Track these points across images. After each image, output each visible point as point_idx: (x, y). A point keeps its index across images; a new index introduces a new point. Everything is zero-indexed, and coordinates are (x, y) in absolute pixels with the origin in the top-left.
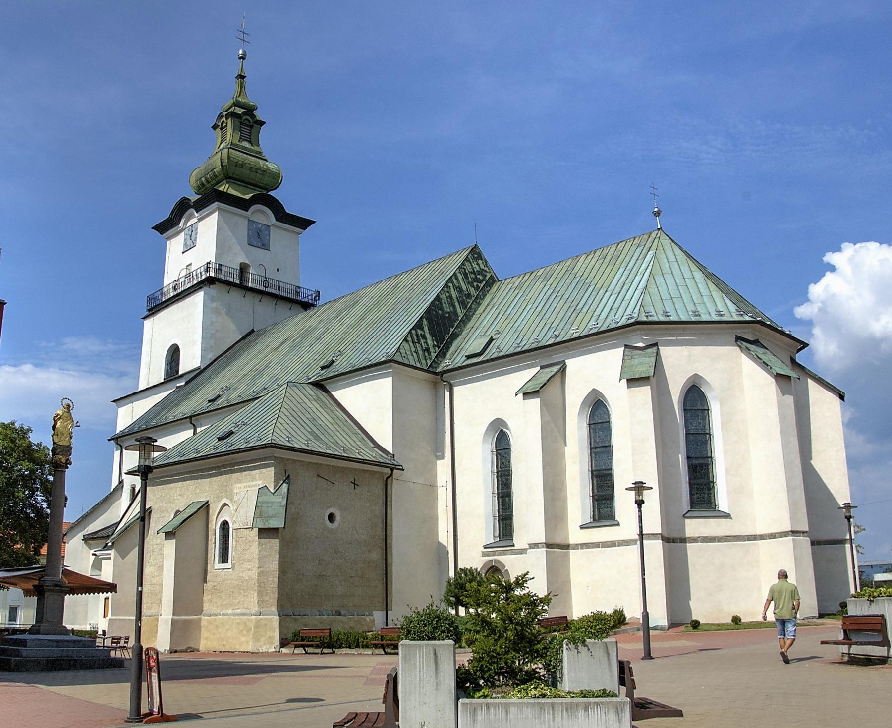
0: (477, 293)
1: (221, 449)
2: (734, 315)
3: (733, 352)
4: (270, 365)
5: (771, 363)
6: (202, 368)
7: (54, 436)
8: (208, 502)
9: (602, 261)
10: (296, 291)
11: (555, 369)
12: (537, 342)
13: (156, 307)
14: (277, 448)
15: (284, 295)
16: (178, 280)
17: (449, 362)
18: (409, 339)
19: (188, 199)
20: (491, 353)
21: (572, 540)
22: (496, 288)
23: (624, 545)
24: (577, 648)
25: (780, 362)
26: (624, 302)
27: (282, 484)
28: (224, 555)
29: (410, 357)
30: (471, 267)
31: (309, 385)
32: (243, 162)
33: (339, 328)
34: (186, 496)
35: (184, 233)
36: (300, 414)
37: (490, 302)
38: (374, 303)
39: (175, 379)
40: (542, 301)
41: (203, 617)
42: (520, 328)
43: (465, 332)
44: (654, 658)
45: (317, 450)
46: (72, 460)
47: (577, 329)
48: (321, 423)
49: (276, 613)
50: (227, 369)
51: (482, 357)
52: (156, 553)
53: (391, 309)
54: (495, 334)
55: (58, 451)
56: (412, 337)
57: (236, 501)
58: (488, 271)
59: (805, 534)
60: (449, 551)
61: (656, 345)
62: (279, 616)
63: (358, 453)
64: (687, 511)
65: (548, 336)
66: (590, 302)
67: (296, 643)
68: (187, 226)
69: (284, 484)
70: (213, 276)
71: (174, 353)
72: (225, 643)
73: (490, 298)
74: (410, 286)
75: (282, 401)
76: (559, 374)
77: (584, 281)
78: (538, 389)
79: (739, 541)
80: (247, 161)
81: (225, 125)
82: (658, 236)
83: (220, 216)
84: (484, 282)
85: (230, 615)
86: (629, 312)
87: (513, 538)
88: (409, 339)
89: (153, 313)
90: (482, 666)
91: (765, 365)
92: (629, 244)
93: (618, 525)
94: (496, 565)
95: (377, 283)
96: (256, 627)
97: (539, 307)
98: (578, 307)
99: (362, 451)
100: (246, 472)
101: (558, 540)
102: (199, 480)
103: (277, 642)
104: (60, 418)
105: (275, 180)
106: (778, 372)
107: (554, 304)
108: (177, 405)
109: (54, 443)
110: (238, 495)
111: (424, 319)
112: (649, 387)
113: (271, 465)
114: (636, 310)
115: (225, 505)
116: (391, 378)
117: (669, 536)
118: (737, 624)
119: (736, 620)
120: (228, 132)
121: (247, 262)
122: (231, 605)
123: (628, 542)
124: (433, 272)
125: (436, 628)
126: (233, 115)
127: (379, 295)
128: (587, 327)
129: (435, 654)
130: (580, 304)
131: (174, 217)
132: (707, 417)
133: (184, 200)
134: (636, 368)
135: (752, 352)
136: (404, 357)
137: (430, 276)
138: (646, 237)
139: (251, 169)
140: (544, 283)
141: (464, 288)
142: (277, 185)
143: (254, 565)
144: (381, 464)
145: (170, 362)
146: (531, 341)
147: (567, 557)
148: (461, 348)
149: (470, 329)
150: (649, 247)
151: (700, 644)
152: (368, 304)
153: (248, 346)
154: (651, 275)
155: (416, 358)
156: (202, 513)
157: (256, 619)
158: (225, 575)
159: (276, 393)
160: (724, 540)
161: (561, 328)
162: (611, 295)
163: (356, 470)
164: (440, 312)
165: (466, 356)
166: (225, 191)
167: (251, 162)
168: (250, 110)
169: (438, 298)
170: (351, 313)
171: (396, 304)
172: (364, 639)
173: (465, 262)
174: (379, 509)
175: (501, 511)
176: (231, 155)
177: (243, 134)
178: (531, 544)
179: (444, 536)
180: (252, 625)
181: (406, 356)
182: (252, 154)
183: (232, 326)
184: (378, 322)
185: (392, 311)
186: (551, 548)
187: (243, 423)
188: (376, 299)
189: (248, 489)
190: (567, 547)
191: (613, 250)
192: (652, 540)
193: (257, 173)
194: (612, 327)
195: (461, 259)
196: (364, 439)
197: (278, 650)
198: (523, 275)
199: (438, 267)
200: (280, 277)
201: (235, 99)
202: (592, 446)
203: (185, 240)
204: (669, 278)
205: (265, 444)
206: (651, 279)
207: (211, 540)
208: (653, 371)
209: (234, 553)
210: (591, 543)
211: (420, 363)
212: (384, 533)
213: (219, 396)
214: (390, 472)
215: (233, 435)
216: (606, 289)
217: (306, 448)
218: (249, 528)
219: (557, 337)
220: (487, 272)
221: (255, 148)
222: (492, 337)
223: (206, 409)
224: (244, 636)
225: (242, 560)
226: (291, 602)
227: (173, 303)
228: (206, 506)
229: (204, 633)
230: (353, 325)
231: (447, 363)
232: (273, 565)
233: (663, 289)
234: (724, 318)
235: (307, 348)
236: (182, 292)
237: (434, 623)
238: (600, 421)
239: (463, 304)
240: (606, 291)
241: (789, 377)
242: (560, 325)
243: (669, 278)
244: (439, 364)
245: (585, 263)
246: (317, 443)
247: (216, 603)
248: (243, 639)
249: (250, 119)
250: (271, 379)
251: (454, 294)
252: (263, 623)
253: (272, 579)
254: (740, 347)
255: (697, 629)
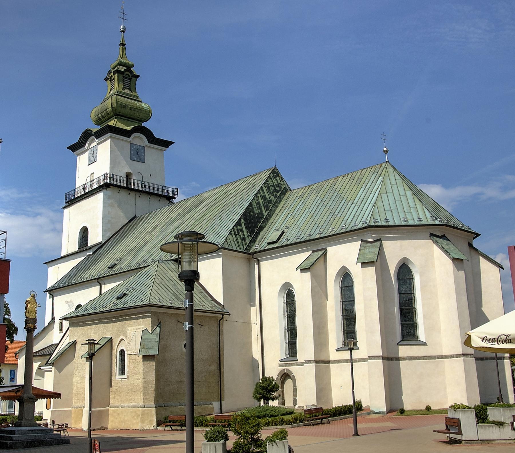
0: (276, 199)
1: (119, 306)
2: (429, 220)
3: (429, 243)
4: (147, 244)
5: (451, 251)
6: (103, 242)
7: (26, 313)
8: (111, 338)
9: (352, 181)
10: (163, 189)
11: (321, 253)
12: (310, 236)
13: (72, 201)
14: (153, 306)
15: (155, 192)
16: (85, 184)
17: (257, 247)
18: (233, 233)
19: (91, 130)
20: (283, 242)
21: (332, 358)
22: (287, 195)
23: (362, 362)
24: (272, 444)
25: (457, 249)
26: (362, 211)
27: (156, 327)
28: (122, 370)
29: (233, 245)
30: (272, 182)
31: (172, 261)
32: (126, 104)
33: (190, 221)
34: (98, 334)
35: (88, 152)
36: (166, 282)
37: (284, 205)
38: (212, 204)
39: (86, 250)
40: (315, 207)
41: (110, 408)
42: (301, 225)
43: (268, 226)
44: (359, 435)
45: (177, 306)
46: (37, 326)
47: (333, 229)
48: (179, 287)
49: (154, 406)
50: (119, 245)
51: (277, 244)
52: (80, 369)
53: (222, 210)
54: (285, 229)
55: (29, 321)
56: (234, 231)
57: (129, 338)
58: (283, 184)
59: (472, 355)
60: (260, 363)
61: (380, 240)
62: (156, 407)
63: (202, 306)
64: (400, 341)
65: (316, 232)
66: (342, 210)
67: (166, 424)
68: (90, 147)
69: (157, 327)
70: (109, 182)
71: (84, 232)
72: (123, 424)
73: (284, 203)
74: (234, 193)
75: (155, 274)
76: (323, 256)
77: (340, 194)
78: (309, 267)
79: (432, 359)
80: (128, 104)
81: (113, 78)
82: (386, 166)
83: (112, 142)
84: (280, 192)
85: (126, 407)
86: (364, 219)
87: (297, 355)
88: (233, 233)
89: (69, 205)
90: (236, 450)
91: (446, 252)
92: (369, 170)
93: (358, 349)
94: (287, 372)
95: (214, 189)
96: (142, 414)
97: (312, 211)
98: (335, 214)
99: (205, 304)
100: (135, 320)
101: (323, 358)
102: (106, 324)
103: (155, 423)
104: (30, 302)
105: (147, 115)
106: (454, 257)
107: (322, 210)
108: (88, 268)
109: (26, 317)
110: (130, 334)
111: (242, 219)
112: (374, 267)
113: (149, 316)
114: (369, 218)
115: (122, 340)
116: (221, 258)
117: (388, 357)
118: (429, 411)
119: (428, 408)
120: (115, 83)
121: (131, 171)
122: (127, 401)
123: (364, 360)
124: (249, 185)
125: (218, 435)
126: (118, 72)
127: (215, 199)
128: (339, 228)
129: (215, 447)
130: (336, 211)
131: (82, 141)
132: (412, 283)
133: (88, 130)
134: (367, 255)
135: (439, 244)
136: (230, 245)
137: (247, 187)
138: (379, 166)
139: (131, 109)
140: (316, 194)
141: (267, 196)
142: (148, 118)
143: (140, 376)
144: (216, 312)
145: (82, 237)
146: (306, 235)
147: (329, 368)
148: (265, 236)
149: (270, 224)
150: (380, 174)
151: (395, 425)
152: (208, 204)
153: (133, 228)
154: (380, 194)
155: (237, 245)
156: (108, 345)
157: (142, 410)
158: (123, 382)
159: (152, 268)
160: (422, 359)
161: (325, 227)
162: (355, 206)
163: (200, 316)
164: (252, 214)
165: (268, 243)
166: (114, 125)
167: (131, 104)
168: (129, 68)
169: (251, 204)
170: (198, 210)
171: (225, 206)
172: (205, 421)
173: (268, 179)
174: (215, 339)
175: (290, 338)
176: (117, 100)
177: (125, 84)
178: (306, 361)
179: (256, 354)
180: (140, 413)
181: (231, 244)
182: (131, 98)
183: (122, 214)
184: (214, 218)
185: (223, 212)
186: (319, 363)
187: (131, 288)
188: (213, 201)
189: (136, 330)
190: (329, 362)
191: (358, 174)
192: (376, 359)
193: (135, 111)
194: (354, 229)
195: (266, 177)
196: (206, 296)
197: (155, 428)
198: (304, 188)
199: (252, 181)
200: (152, 180)
201: (119, 61)
202: (343, 301)
203: (89, 157)
204: (390, 195)
205: (146, 304)
206: (379, 196)
207: (114, 361)
208: (376, 258)
209: (128, 369)
210: (343, 360)
211: (239, 247)
212: (219, 354)
213: (115, 265)
214: (222, 316)
215: (126, 296)
216: (352, 202)
217: (170, 305)
218: (137, 354)
219: (322, 233)
220: (282, 185)
221: (133, 94)
222: (283, 231)
223: (107, 274)
224: (135, 419)
225: (133, 373)
226: (163, 398)
227: (83, 199)
228: (110, 340)
229: (111, 418)
230: (198, 220)
231: (256, 247)
232: (152, 377)
233: (386, 203)
234: (423, 223)
235: (171, 233)
236: (89, 192)
237: (217, 433)
238: (347, 285)
239: (267, 208)
240: (352, 203)
241: (462, 260)
242: (324, 225)
243: (390, 195)
244: (251, 247)
245: (342, 182)
246: (177, 301)
247: (118, 399)
248: (135, 421)
249: (129, 74)
250: (148, 254)
251: (261, 201)
252: (146, 412)
253: (151, 386)
254: (433, 241)
255: (403, 414)
